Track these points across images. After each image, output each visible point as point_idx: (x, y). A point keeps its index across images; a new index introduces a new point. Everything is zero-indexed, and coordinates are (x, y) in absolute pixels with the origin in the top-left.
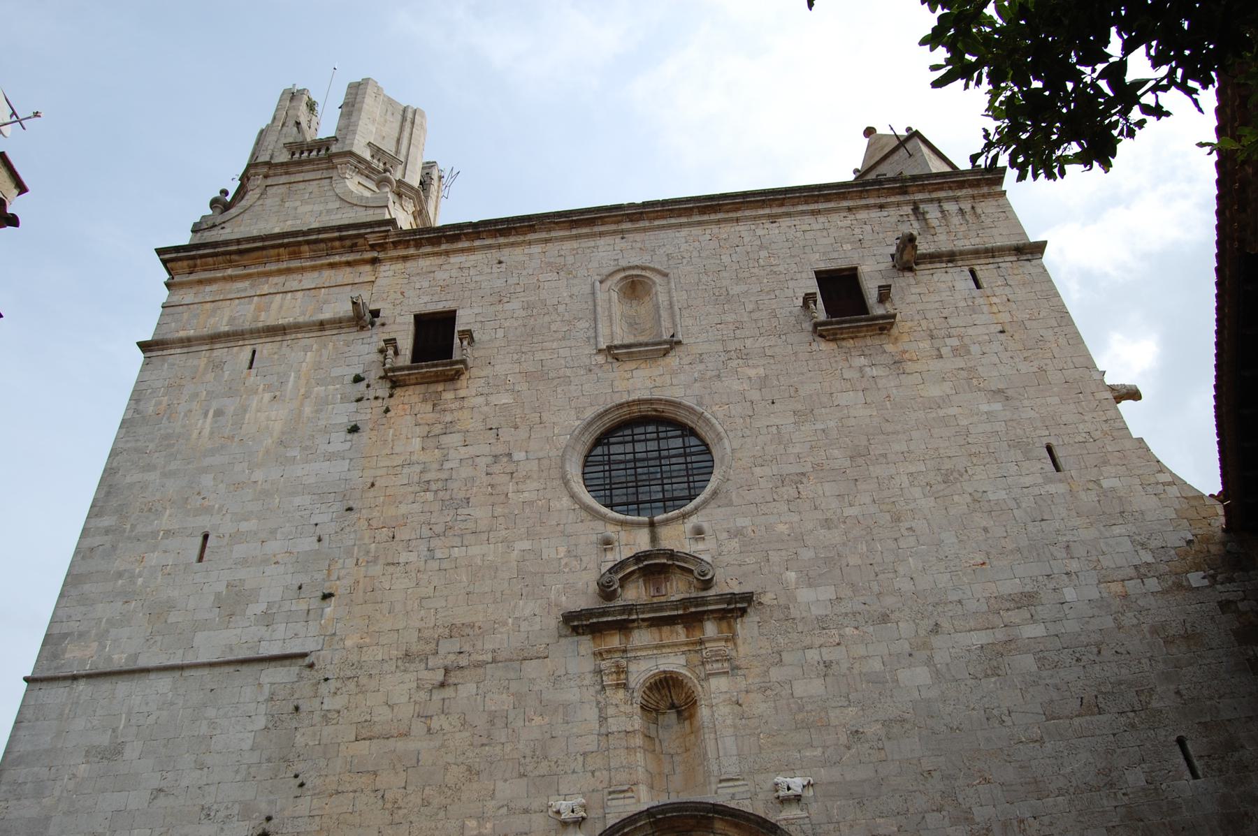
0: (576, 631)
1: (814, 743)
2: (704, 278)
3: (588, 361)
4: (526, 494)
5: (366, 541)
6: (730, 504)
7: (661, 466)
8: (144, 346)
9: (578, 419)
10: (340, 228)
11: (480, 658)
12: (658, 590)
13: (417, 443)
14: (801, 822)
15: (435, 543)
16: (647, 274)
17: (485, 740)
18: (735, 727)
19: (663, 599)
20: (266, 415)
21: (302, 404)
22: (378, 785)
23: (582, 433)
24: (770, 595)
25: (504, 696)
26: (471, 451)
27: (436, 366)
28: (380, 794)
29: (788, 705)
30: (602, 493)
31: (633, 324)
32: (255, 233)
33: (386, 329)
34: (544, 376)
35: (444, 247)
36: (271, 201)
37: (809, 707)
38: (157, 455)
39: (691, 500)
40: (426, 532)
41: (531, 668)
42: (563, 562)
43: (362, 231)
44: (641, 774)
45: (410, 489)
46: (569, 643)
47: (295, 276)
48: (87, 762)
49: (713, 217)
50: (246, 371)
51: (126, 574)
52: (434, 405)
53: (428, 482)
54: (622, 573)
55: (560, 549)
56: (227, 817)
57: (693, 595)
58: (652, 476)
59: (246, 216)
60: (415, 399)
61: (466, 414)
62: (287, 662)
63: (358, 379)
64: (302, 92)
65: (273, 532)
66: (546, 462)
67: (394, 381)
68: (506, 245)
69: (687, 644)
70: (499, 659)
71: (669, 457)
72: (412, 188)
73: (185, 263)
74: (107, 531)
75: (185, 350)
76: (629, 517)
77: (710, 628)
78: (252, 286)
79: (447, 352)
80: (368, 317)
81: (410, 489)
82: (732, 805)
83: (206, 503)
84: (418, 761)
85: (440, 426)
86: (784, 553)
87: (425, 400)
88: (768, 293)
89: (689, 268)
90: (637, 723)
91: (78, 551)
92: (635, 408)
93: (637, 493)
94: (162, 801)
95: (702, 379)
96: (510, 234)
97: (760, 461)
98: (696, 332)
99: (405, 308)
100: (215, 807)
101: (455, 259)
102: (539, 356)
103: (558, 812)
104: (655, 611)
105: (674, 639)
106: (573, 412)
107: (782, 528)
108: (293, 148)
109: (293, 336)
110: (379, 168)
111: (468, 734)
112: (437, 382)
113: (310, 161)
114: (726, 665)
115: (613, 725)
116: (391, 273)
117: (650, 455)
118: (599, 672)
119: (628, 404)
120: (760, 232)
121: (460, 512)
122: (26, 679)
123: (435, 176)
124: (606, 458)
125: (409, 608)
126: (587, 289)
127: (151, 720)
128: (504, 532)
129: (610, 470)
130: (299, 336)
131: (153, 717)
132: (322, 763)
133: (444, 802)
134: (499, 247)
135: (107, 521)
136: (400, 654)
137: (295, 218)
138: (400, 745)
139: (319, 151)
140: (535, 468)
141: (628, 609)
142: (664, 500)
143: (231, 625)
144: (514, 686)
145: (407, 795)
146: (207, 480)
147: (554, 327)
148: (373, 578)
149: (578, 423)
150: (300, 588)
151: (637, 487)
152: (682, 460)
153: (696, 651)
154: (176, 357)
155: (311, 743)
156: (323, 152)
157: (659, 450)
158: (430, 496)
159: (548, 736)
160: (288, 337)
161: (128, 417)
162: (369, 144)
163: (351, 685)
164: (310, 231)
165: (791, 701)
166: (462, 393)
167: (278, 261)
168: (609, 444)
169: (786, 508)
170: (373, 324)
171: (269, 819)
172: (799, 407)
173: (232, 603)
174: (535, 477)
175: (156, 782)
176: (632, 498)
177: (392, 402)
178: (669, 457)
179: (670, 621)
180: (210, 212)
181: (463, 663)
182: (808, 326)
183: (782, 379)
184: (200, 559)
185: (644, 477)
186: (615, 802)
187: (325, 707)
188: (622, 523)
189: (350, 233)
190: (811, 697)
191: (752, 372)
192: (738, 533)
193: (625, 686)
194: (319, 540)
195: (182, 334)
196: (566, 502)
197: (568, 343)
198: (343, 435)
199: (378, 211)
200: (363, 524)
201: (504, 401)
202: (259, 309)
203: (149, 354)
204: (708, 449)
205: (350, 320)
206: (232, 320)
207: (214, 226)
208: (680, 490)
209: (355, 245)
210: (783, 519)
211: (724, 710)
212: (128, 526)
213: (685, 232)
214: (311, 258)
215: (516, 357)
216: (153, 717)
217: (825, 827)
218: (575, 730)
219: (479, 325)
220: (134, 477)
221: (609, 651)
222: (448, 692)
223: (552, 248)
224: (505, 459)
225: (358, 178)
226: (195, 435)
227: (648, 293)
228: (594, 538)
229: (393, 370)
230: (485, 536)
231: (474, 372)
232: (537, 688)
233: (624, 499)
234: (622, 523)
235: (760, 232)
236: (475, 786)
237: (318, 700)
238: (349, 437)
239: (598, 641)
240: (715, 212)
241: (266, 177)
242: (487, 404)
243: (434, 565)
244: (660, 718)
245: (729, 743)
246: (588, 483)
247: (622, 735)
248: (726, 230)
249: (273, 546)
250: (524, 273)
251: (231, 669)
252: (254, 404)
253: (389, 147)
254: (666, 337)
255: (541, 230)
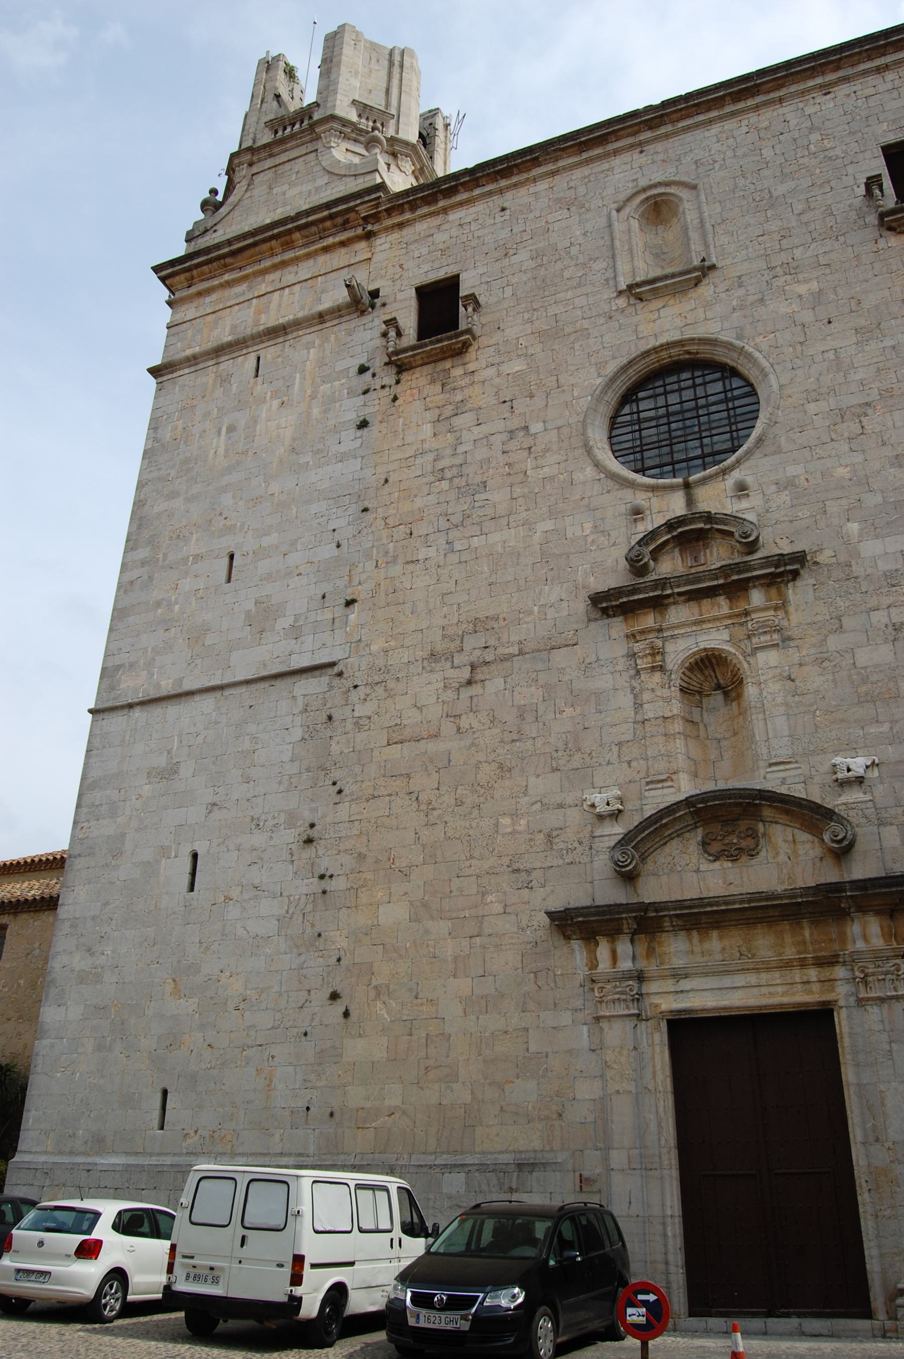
0: (606, 613)
1: (881, 718)
2: (741, 182)
3: (606, 308)
4: (546, 469)
5: (385, 541)
6: (778, 451)
7: (698, 417)
8: (155, 372)
9: (599, 376)
10: (328, 205)
11: (507, 651)
12: (696, 559)
13: (428, 429)
14: (863, 806)
15: (454, 534)
16: (671, 190)
17: (515, 737)
18: (786, 704)
19: (701, 569)
20: (277, 423)
21: (310, 407)
22: (412, 787)
23: (604, 391)
24: (828, 553)
25: (533, 689)
26: (485, 429)
27: (440, 341)
28: (414, 797)
29: (850, 676)
30: (632, 457)
31: (659, 255)
32: (246, 229)
33: (388, 309)
34: (562, 329)
35: (441, 204)
36: (259, 191)
37: (874, 678)
38: (179, 480)
39: (734, 452)
40: (444, 525)
41: (560, 657)
42: (590, 539)
43: (352, 204)
44: (681, 761)
45: (424, 480)
46: (599, 627)
47: (290, 268)
48: (150, 783)
49: (750, 102)
50: (252, 381)
51: (164, 602)
52: (443, 385)
53: (442, 470)
54: (655, 544)
55: (586, 525)
56: (274, 826)
57: (737, 561)
58: (688, 431)
59: (236, 213)
60: (423, 381)
61: (477, 389)
62: (317, 673)
63: (363, 370)
64: (277, 58)
65: (293, 543)
66: (565, 431)
67: (400, 365)
68: (508, 188)
69: (730, 617)
70: (526, 650)
71: (707, 406)
72: (407, 144)
73: (182, 277)
74: (143, 564)
75: (193, 369)
76: (661, 481)
77: (757, 597)
78: (250, 288)
79: (454, 323)
80: (366, 299)
81: (424, 480)
82: (783, 790)
83: (228, 523)
84: (450, 761)
85: (450, 407)
86: (844, 502)
87: (433, 382)
88: (821, 186)
89: (722, 173)
90: (676, 707)
91: (120, 586)
92: (664, 354)
93: (672, 453)
94: (217, 814)
95: (742, 307)
96: (512, 174)
97: (814, 395)
98: (733, 253)
99: (405, 283)
100: (263, 817)
101: (454, 216)
102: (552, 310)
103: (593, 806)
104: (692, 583)
105: (715, 613)
106: (593, 369)
107: (842, 472)
108: (275, 125)
109: (295, 334)
110: (369, 128)
111: (498, 731)
112: (444, 359)
113: (292, 136)
114: (775, 636)
115: (650, 711)
116: (387, 246)
117: (687, 406)
118: (632, 655)
119: (656, 350)
120: (809, 110)
121: (477, 497)
122: (90, 711)
123: (440, 125)
124: (635, 416)
125: (431, 606)
126: (603, 222)
127: (200, 740)
128: (524, 514)
129: (640, 430)
130: (301, 333)
131: (201, 737)
132: (358, 769)
133: (477, 801)
134: (501, 191)
135: (142, 553)
136: (425, 654)
137: (285, 204)
138: (431, 747)
139: (302, 122)
140: (555, 439)
141: (662, 583)
142: (703, 456)
143: (263, 641)
144: (543, 678)
145: (440, 795)
146: (227, 500)
147: (567, 274)
148: (393, 578)
149: (599, 381)
150: (324, 597)
151: (671, 445)
152: (723, 407)
153: (741, 624)
154: (185, 378)
155: (346, 751)
156: (306, 122)
157: (696, 399)
158: (445, 485)
159: (580, 727)
160: (290, 337)
161: (148, 447)
162: (354, 102)
163: (380, 690)
164: (299, 215)
165: (853, 672)
166: (471, 367)
167: (272, 255)
168: (638, 400)
169: (847, 448)
170: (373, 306)
171: (312, 826)
172: (863, 322)
173: (262, 619)
174: (555, 448)
175: (210, 799)
176: (667, 459)
177: (399, 389)
178: (707, 406)
179: (711, 593)
180: (202, 216)
181: (489, 657)
182: (872, 219)
183: (839, 290)
184: (229, 580)
185: (679, 433)
186: (652, 793)
187: (356, 714)
188: (653, 489)
189: (340, 208)
190: (878, 666)
191: (802, 289)
192: (789, 484)
193: (661, 668)
194: (338, 546)
195: (189, 352)
196: (590, 471)
197: (584, 290)
198: (352, 432)
199: (368, 177)
200: (380, 523)
201: (519, 368)
202: (259, 312)
203: (160, 379)
204: (754, 390)
205: (348, 306)
206: (234, 327)
207: (206, 231)
208: (721, 441)
209: (347, 221)
210: (843, 462)
211: (774, 687)
212: (161, 556)
213: (715, 129)
214: (305, 245)
215: (526, 316)
216: (201, 737)
217: (892, 811)
218: (608, 720)
219: (485, 286)
220: (161, 506)
221: (642, 632)
222: (476, 689)
223: (561, 181)
224: (522, 434)
225: (345, 145)
226: (211, 456)
227: (675, 214)
228: (622, 509)
229: (397, 353)
230: (504, 521)
231: (483, 341)
232: (566, 678)
233: (657, 461)
234: (653, 489)
235: (809, 110)
236: (507, 783)
237: (350, 707)
238: (359, 433)
239: (631, 622)
240: (753, 96)
241: (251, 165)
242: (499, 375)
243: (454, 558)
244: (705, 700)
245: (780, 723)
246: (616, 447)
247: (660, 721)
248: (766, 117)
249: (295, 558)
250: (531, 216)
251: (262, 685)
252: (264, 414)
253: (377, 101)
254: (696, 262)
255: (546, 162)
